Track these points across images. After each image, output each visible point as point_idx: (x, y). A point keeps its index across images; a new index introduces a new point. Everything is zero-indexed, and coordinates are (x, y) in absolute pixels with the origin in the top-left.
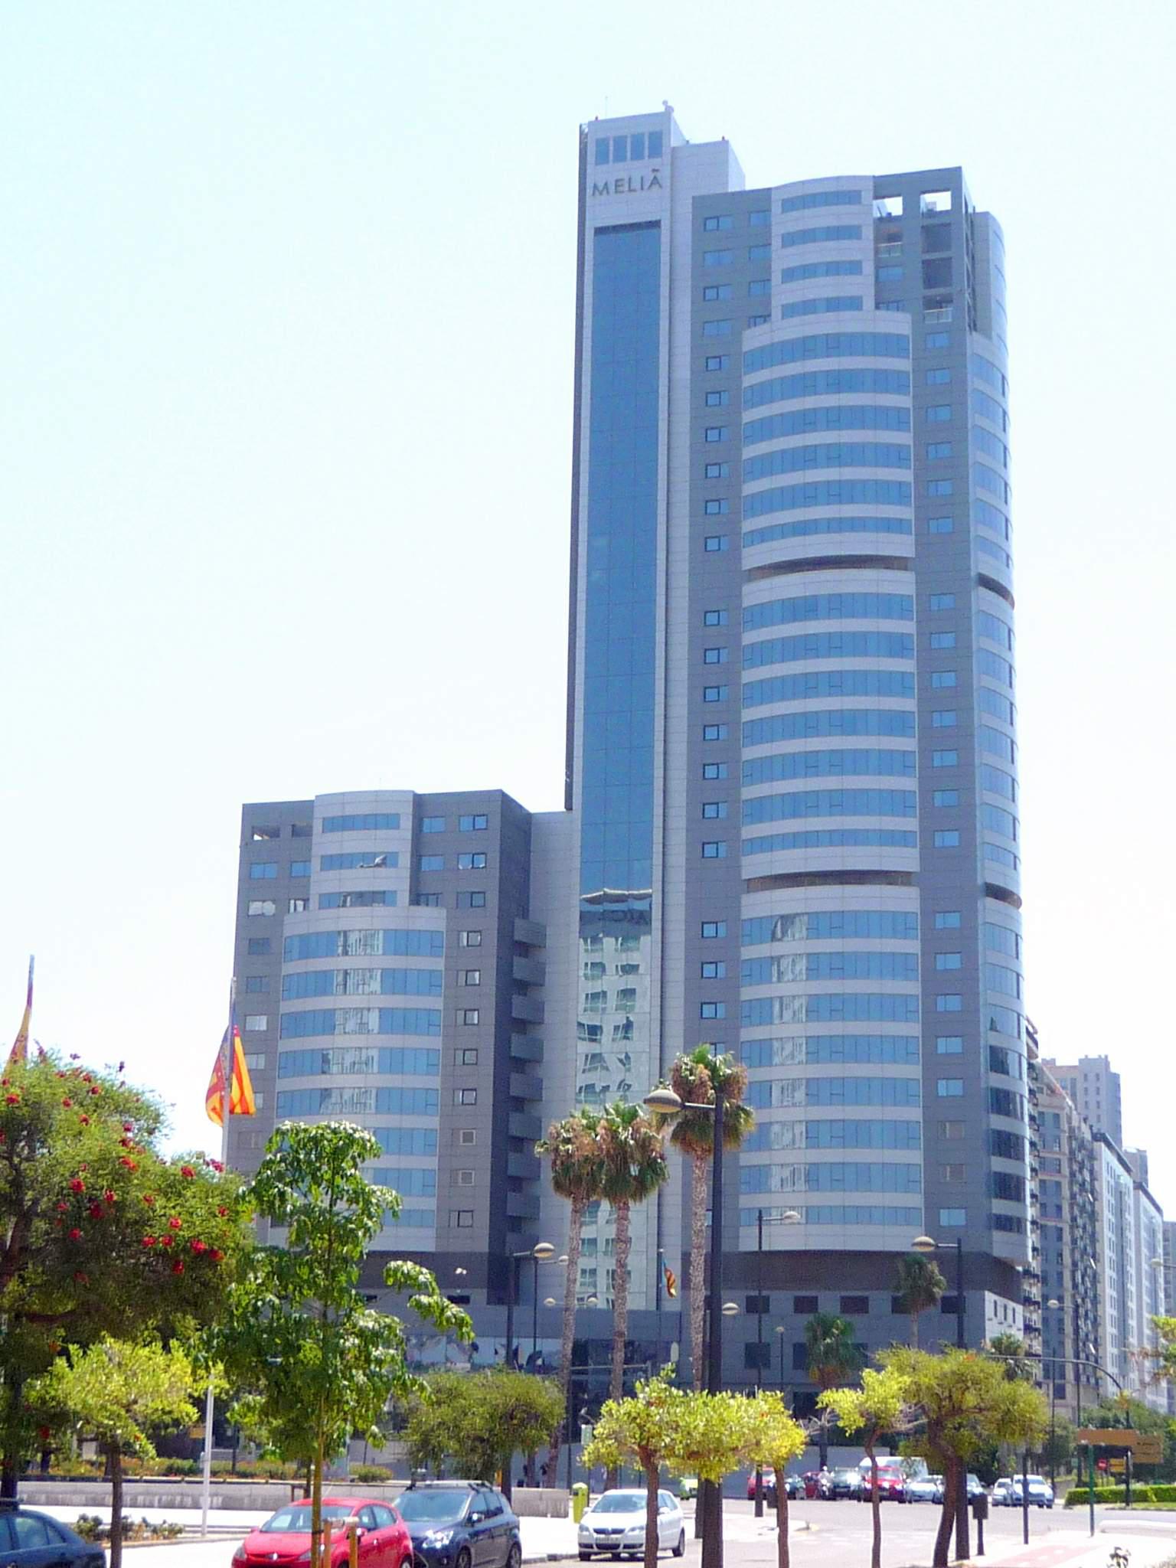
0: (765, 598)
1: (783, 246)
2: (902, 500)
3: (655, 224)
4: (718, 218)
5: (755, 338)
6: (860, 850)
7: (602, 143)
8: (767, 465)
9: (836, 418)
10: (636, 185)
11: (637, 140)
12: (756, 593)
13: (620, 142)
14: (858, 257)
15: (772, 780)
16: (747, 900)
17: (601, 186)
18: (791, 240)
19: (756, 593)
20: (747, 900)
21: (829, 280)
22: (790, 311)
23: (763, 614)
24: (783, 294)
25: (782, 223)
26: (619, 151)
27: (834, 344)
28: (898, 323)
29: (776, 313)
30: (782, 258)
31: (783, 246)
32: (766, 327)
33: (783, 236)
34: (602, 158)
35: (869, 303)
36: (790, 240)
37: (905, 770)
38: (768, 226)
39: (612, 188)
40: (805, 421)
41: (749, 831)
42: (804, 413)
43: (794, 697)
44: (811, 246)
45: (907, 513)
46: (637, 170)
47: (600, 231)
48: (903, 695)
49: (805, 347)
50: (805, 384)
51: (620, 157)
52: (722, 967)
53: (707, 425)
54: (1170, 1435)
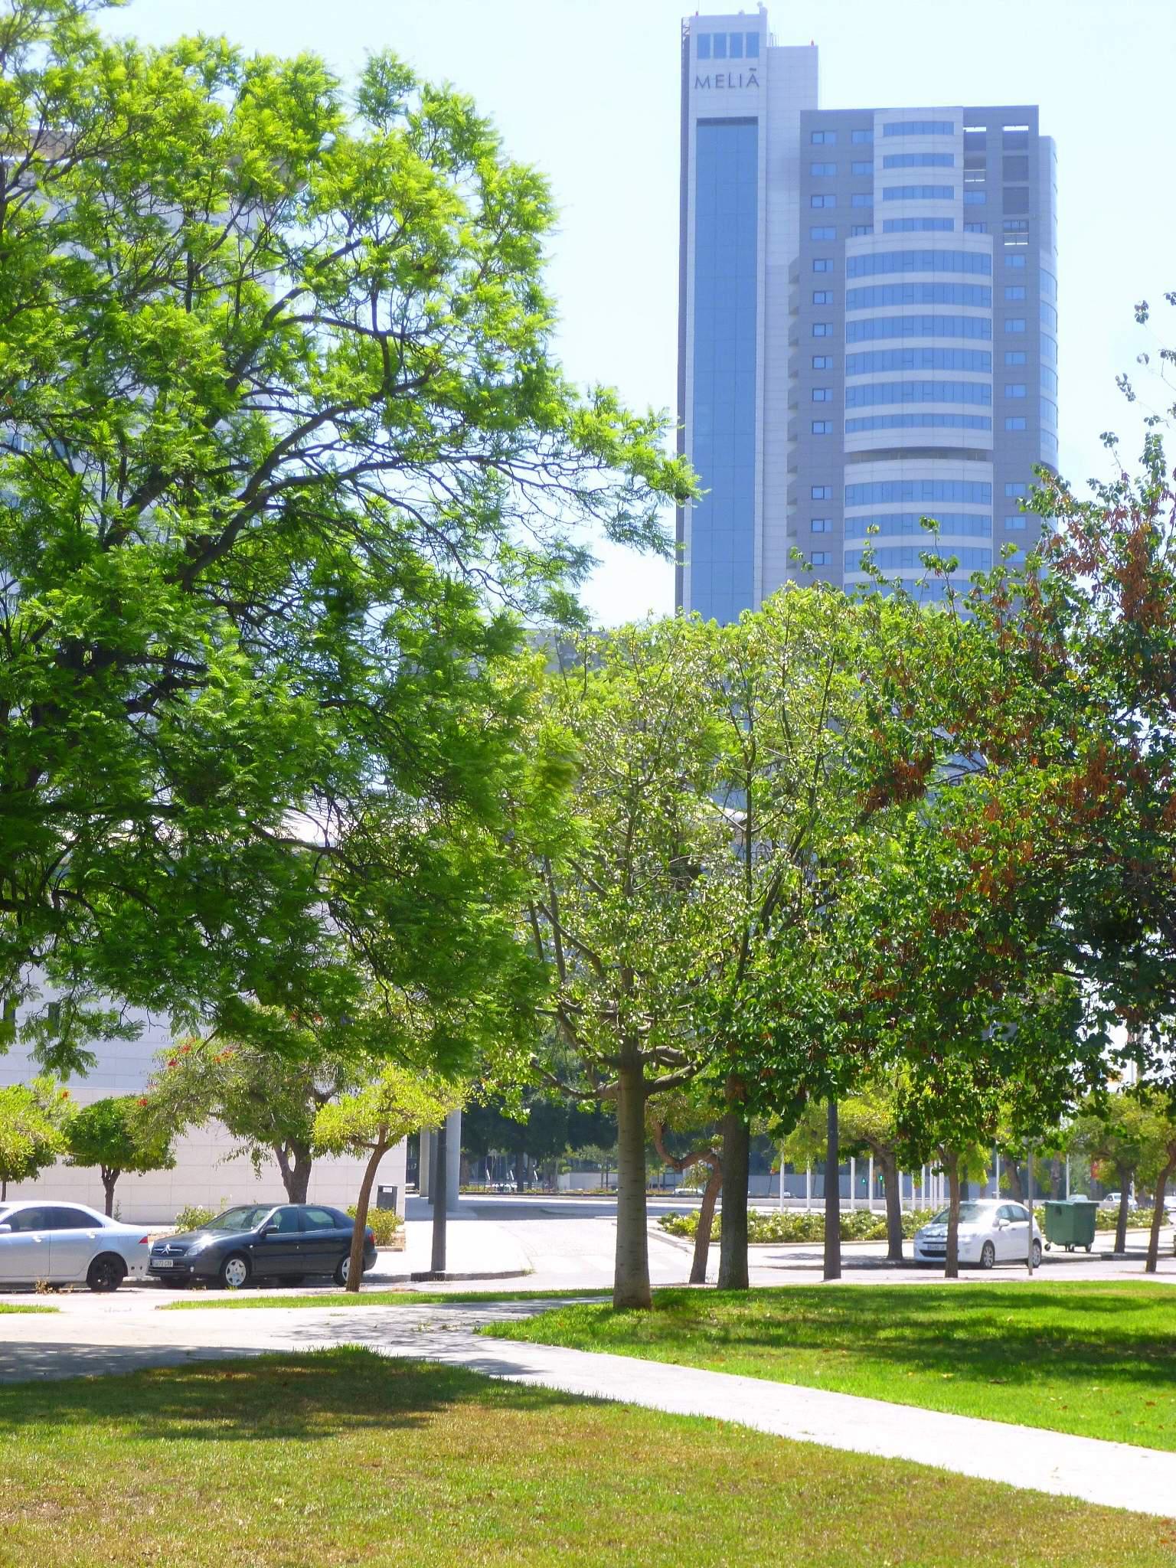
0: (866, 478)
1: (885, 135)
2: (983, 400)
3: (753, 121)
4: (825, 260)
5: (858, 246)
6: (945, 431)
7: (703, 40)
8: (867, 330)
9: (931, 326)
10: (735, 81)
11: (736, 38)
12: (858, 474)
13: (720, 39)
14: (950, 183)
15: (873, 338)
16: (849, 469)
17: (702, 79)
18: (891, 162)
19: (858, 474)
20: (849, 469)
21: (927, 202)
22: (891, 226)
23: (864, 493)
24: (884, 210)
25: (884, 146)
26: (718, 50)
27: (931, 260)
28: (980, 243)
29: (878, 227)
30: (884, 178)
31: (885, 135)
32: (868, 238)
33: (885, 222)
34: (703, 53)
35: (958, 224)
36: (891, 162)
37: (983, 367)
38: (870, 179)
39: (713, 82)
40: (901, 327)
41: (851, 413)
42: (901, 516)
43: (893, 270)
44: (908, 170)
45: (986, 411)
46: (739, 66)
47: (702, 122)
48: (982, 305)
49: (904, 260)
50: (904, 294)
51: (720, 53)
52: (829, 393)
53: (815, 418)
54: (1138, 578)
